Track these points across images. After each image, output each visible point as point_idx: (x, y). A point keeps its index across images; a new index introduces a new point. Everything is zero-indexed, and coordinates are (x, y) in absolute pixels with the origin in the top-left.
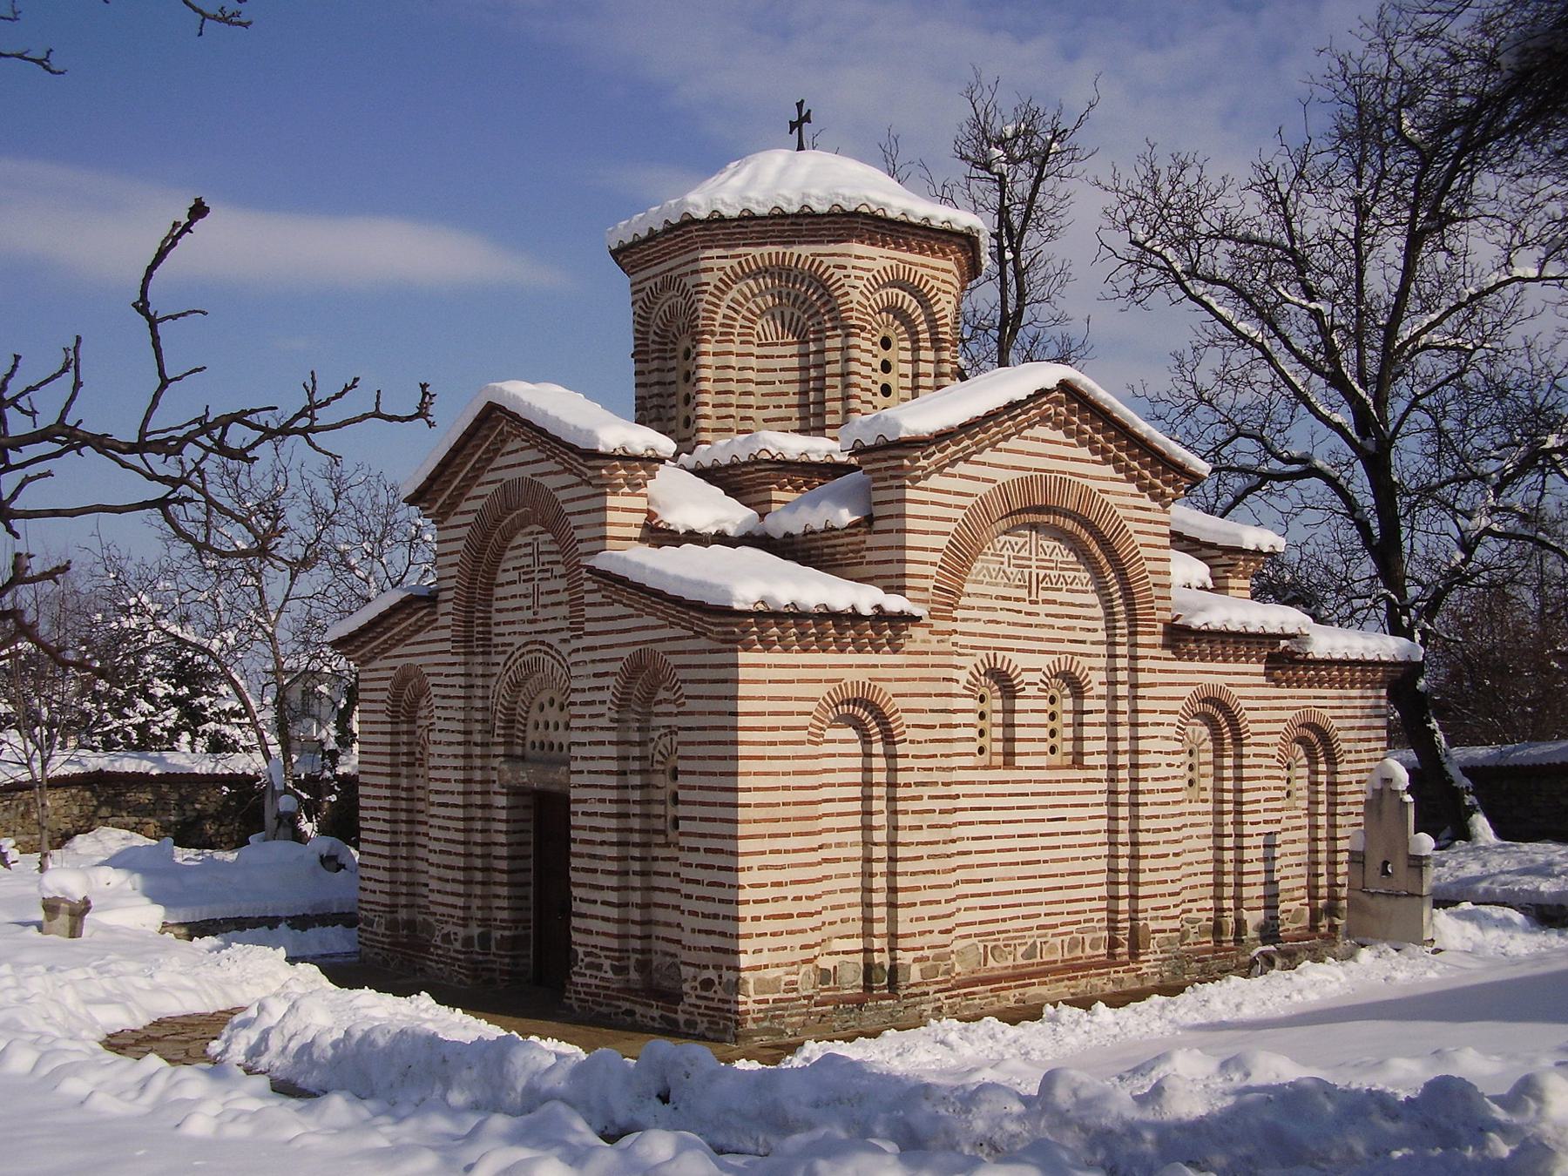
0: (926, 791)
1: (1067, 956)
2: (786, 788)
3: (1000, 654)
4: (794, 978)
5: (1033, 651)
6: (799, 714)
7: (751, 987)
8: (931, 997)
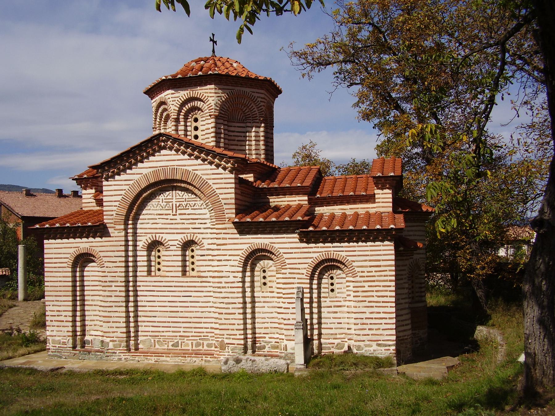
1: (194, 348)
2: (60, 281)
3: (157, 235)
4: (65, 341)
5: (174, 233)
6: (64, 258)
7: (50, 341)
8: (117, 354)
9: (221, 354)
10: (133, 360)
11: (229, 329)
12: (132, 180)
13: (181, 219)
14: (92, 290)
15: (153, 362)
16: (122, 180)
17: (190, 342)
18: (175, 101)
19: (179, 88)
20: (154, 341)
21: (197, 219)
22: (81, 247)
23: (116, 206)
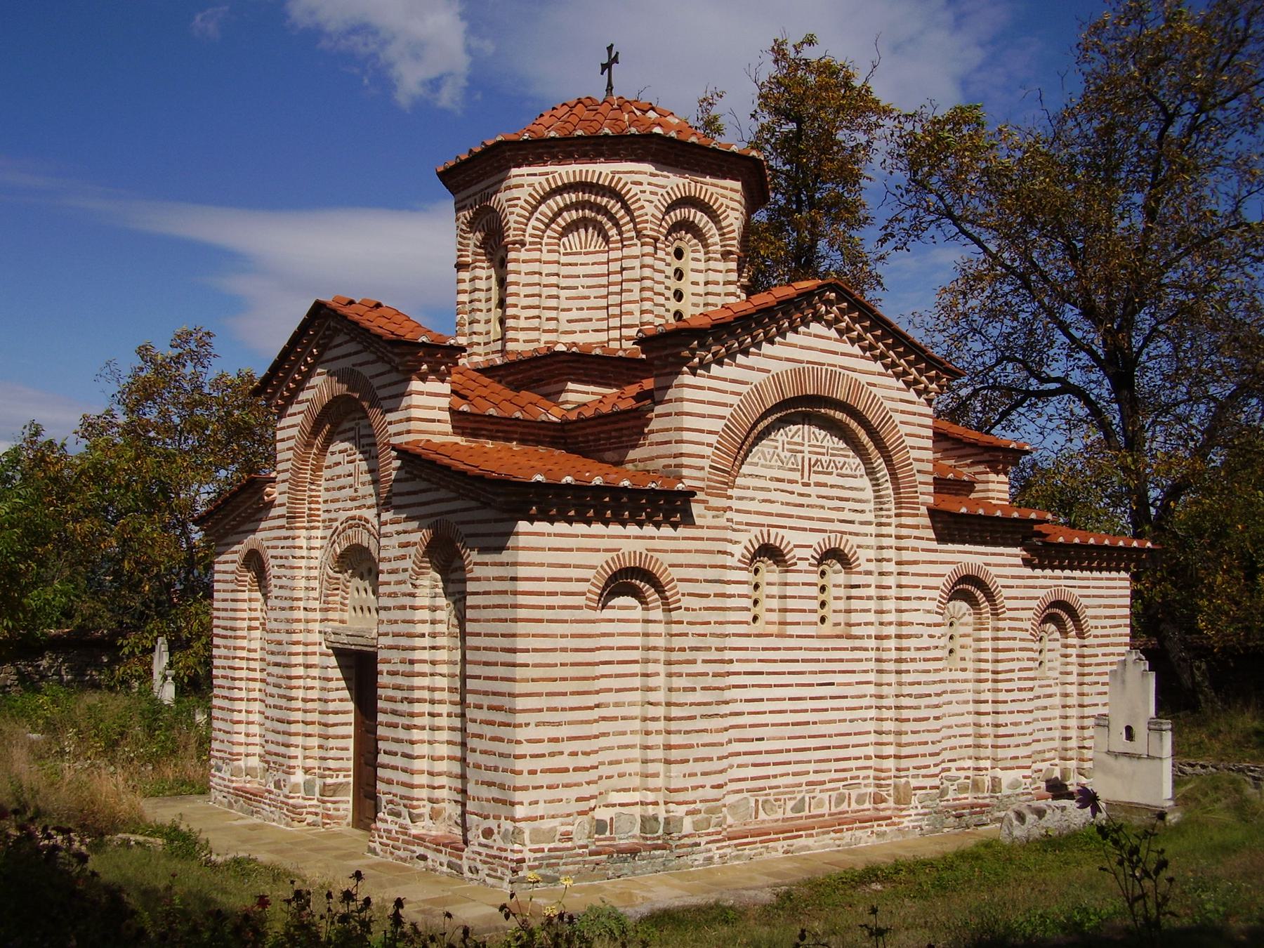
0: (700, 656)
1: (834, 810)
2: (564, 650)
3: (773, 531)
4: (569, 828)
5: (805, 529)
6: (578, 580)
8: (702, 847)
9: (904, 813)
10: (737, 857)
11: (917, 756)
12: (747, 383)
13: (819, 497)
14: (618, 676)
15: (780, 854)
16: (725, 380)
17: (826, 796)
18: (656, 194)
19: (671, 165)
20: (757, 801)
21: (847, 500)
22: (625, 550)
23: (710, 445)
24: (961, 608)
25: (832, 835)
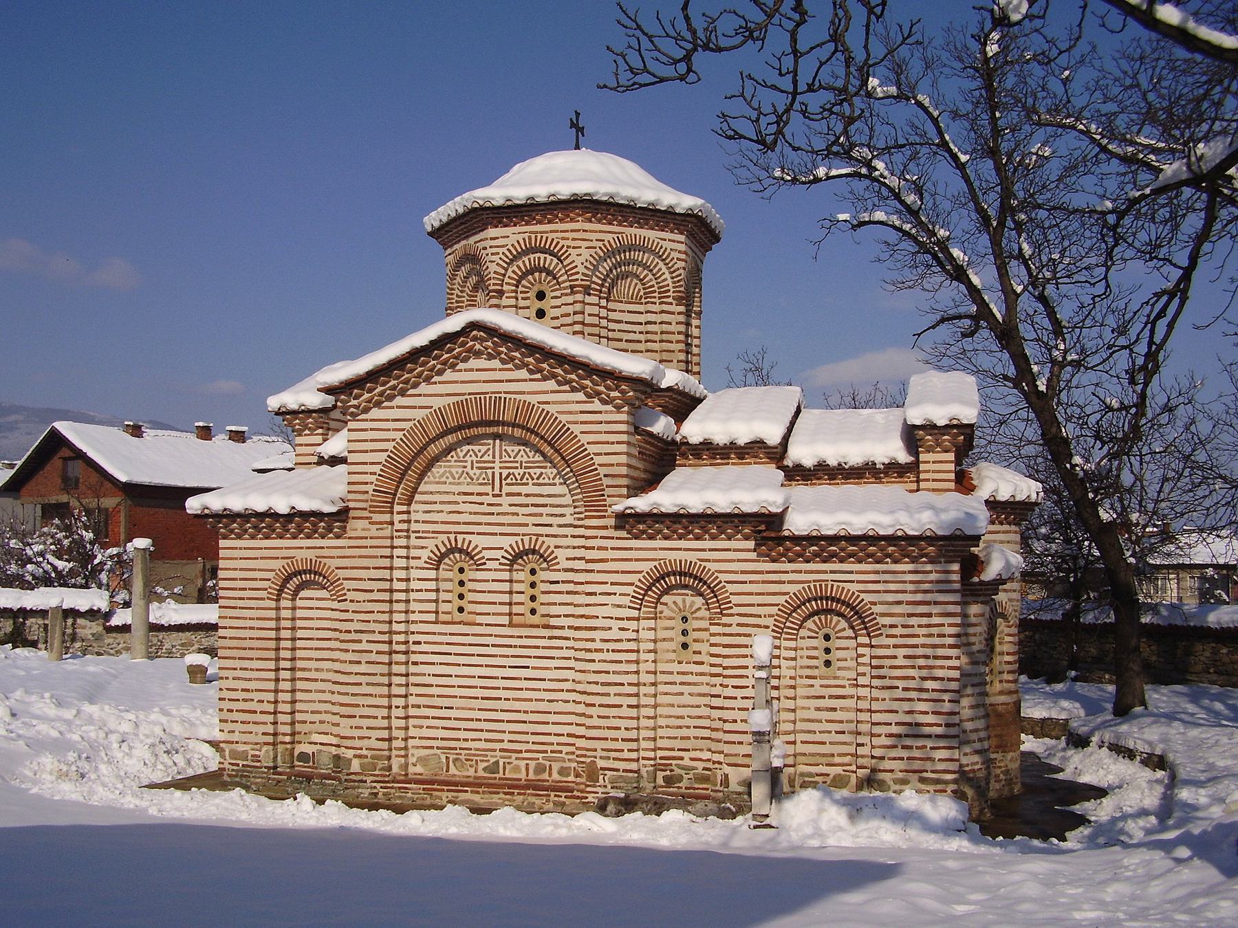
0: (365, 637)
1: (531, 776)
2: (251, 628)
3: (460, 537)
24: (693, 603)
25: (502, 796)
